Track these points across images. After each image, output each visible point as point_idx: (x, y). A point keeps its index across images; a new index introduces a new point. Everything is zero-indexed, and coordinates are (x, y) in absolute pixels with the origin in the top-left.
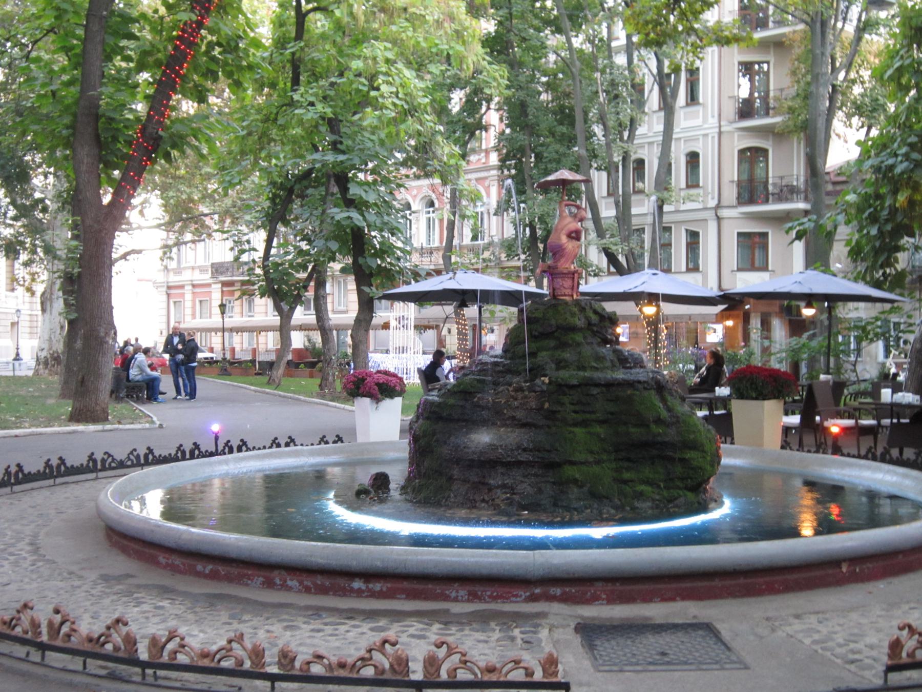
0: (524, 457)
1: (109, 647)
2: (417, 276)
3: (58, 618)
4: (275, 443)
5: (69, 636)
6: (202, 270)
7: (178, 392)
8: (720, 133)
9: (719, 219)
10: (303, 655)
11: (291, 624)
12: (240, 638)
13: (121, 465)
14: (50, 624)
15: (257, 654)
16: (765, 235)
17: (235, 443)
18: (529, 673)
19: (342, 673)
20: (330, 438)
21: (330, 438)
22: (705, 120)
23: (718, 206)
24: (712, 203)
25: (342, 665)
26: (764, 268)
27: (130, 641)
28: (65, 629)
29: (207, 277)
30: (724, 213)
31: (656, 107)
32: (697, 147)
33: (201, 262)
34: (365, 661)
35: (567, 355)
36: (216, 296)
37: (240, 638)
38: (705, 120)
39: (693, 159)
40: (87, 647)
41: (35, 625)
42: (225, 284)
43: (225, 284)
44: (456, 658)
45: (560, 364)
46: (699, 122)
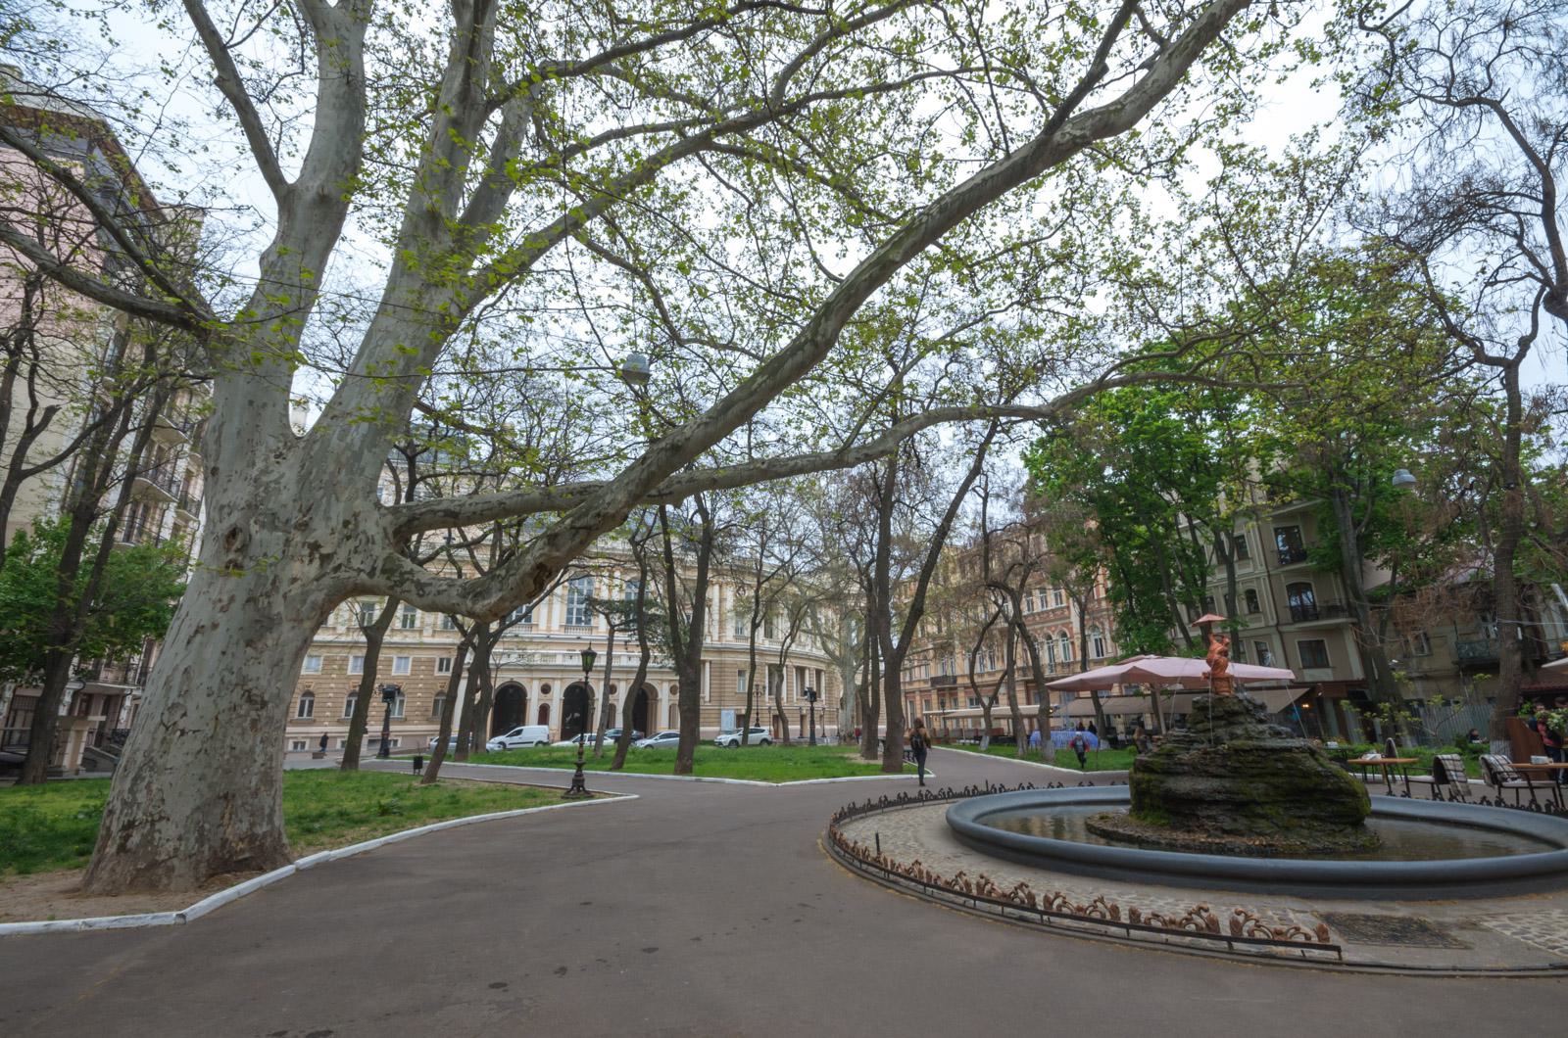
0: (1219, 797)
1: (1017, 900)
2: (1052, 679)
3: (983, 881)
4: (1021, 787)
5: (990, 892)
6: (925, 681)
7: (435, 712)
8: (1269, 576)
9: (1281, 633)
10: (1145, 913)
11: (1005, 879)
12: (1101, 900)
13: (936, 798)
14: (978, 884)
15: (1115, 910)
16: (1320, 643)
17: (997, 786)
18: (1103, 915)
19: (1173, 927)
20: (1055, 784)
21: (1055, 784)
22: (1255, 568)
23: (1278, 625)
24: (1273, 623)
25: (1172, 922)
26: (1326, 666)
27: (1031, 897)
28: (988, 887)
29: (928, 686)
30: (1285, 629)
31: (1214, 560)
32: (1253, 586)
33: (924, 677)
34: (1189, 920)
35: (1239, 731)
36: (934, 697)
37: (1101, 900)
38: (1255, 568)
39: (1251, 595)
40: (1003, 900)
41: (968, 884)
42: (939, 690)
43: (939, 690)
44: (1251, 923)
45: (1233, 736)
46: (1251, 570)
